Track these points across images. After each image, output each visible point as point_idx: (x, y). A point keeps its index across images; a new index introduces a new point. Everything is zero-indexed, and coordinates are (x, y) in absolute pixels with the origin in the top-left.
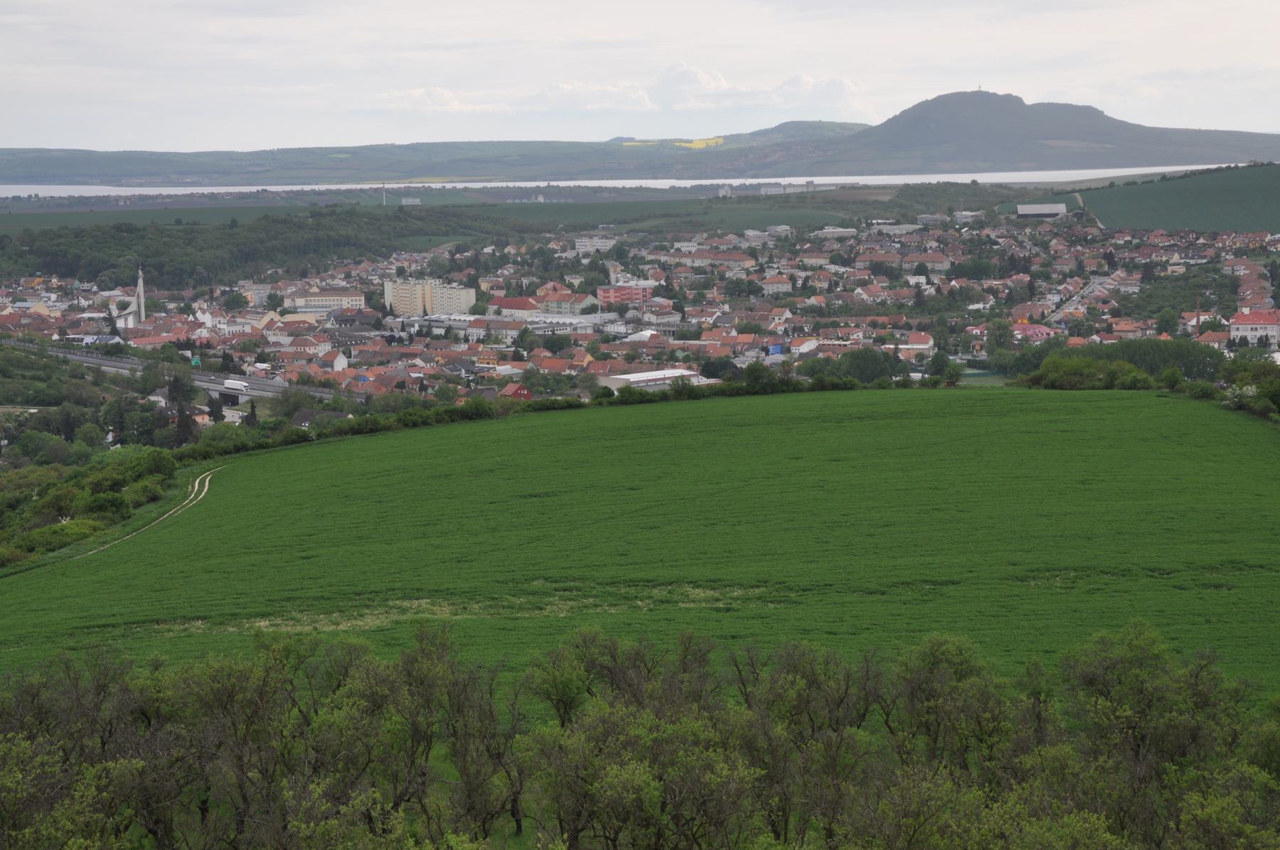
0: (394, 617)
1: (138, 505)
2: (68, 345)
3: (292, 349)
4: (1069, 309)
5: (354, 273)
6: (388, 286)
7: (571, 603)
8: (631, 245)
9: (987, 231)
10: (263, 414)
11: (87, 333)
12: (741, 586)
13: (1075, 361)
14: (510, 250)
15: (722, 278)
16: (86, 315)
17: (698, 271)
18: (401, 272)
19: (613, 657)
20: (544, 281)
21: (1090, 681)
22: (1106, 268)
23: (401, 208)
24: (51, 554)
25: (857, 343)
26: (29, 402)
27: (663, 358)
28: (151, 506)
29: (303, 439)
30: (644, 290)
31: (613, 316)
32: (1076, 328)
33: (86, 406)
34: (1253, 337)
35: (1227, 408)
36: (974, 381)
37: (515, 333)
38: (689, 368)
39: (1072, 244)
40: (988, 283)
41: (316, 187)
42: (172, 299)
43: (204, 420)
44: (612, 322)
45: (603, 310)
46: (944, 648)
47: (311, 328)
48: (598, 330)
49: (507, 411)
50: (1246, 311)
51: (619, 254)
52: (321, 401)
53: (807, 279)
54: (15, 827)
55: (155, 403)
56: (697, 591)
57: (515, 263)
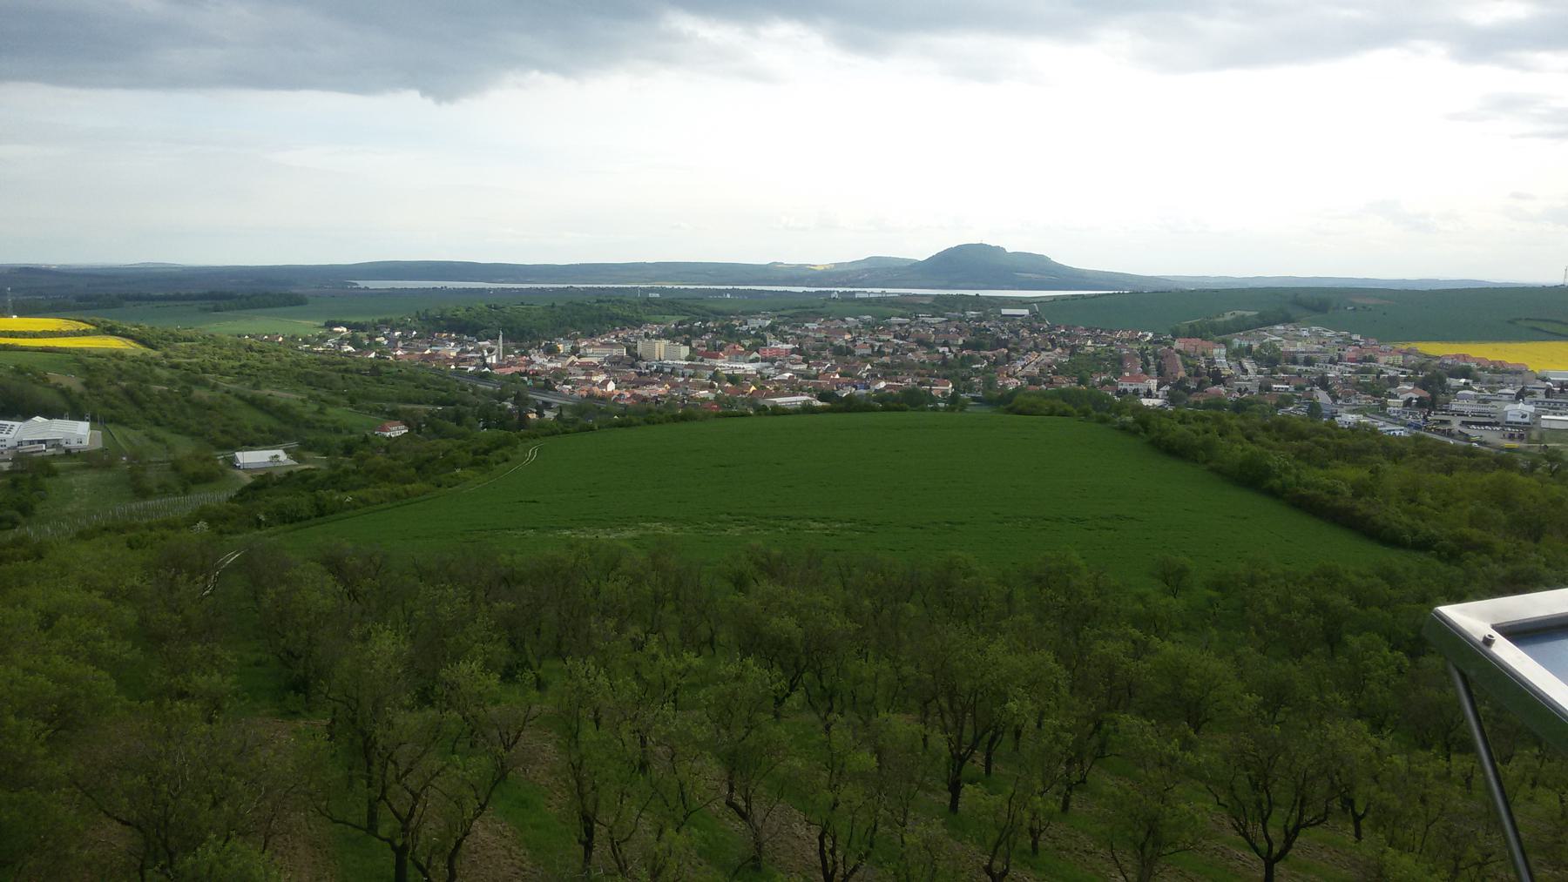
0: (641, 532)
1: (497, 463)
2: (459, 372)
3: (584, 378)
4: (1028, 369)
5: (620, 335)
6: (640, 344)
7: (743, 528)
8: (779, 324)
9: (984, 323)
10: (566, 414)
11: (470, 365)
12: (841, 522)
13: (1033, 399)
14: (710, 324)
15: (831, 344)
16: (469, 355)
17: (819, 340)
18: (647, 335)
19: (769, 560)
20: (729, 343)
21: (1038, 580)
22: (1050, 347)
23: (648, 299)
24: (450, 489)
25: (908, 384)
26: (438, 403)
27: (795, 389)
28: (505, 464)
29: (591, 429)
30: (786, 350)
31: (767, 364)
32: (1032, 380)
33: (468, 406)
34: (1130, 389)
35: (1116, 429)
36: (975, 410)
37: (711, 372)
38: (811, 396)
39: (1032, 332)
40: (983, 353)
41: (601, 286)
42: (517, 348)
43: (533, 416)
44: (767, 367)
45: (762, 361)
46: (958, 559)
47: (595, 366)
48: (759, 372)
49: (706, 417)
50: (1127, 374)
51: (772, 328)
52: (599, 408)
53: (880, 346)
54: (445, 636)
55: (507, 406)
56: (815, 524)
57: (712, 332)
